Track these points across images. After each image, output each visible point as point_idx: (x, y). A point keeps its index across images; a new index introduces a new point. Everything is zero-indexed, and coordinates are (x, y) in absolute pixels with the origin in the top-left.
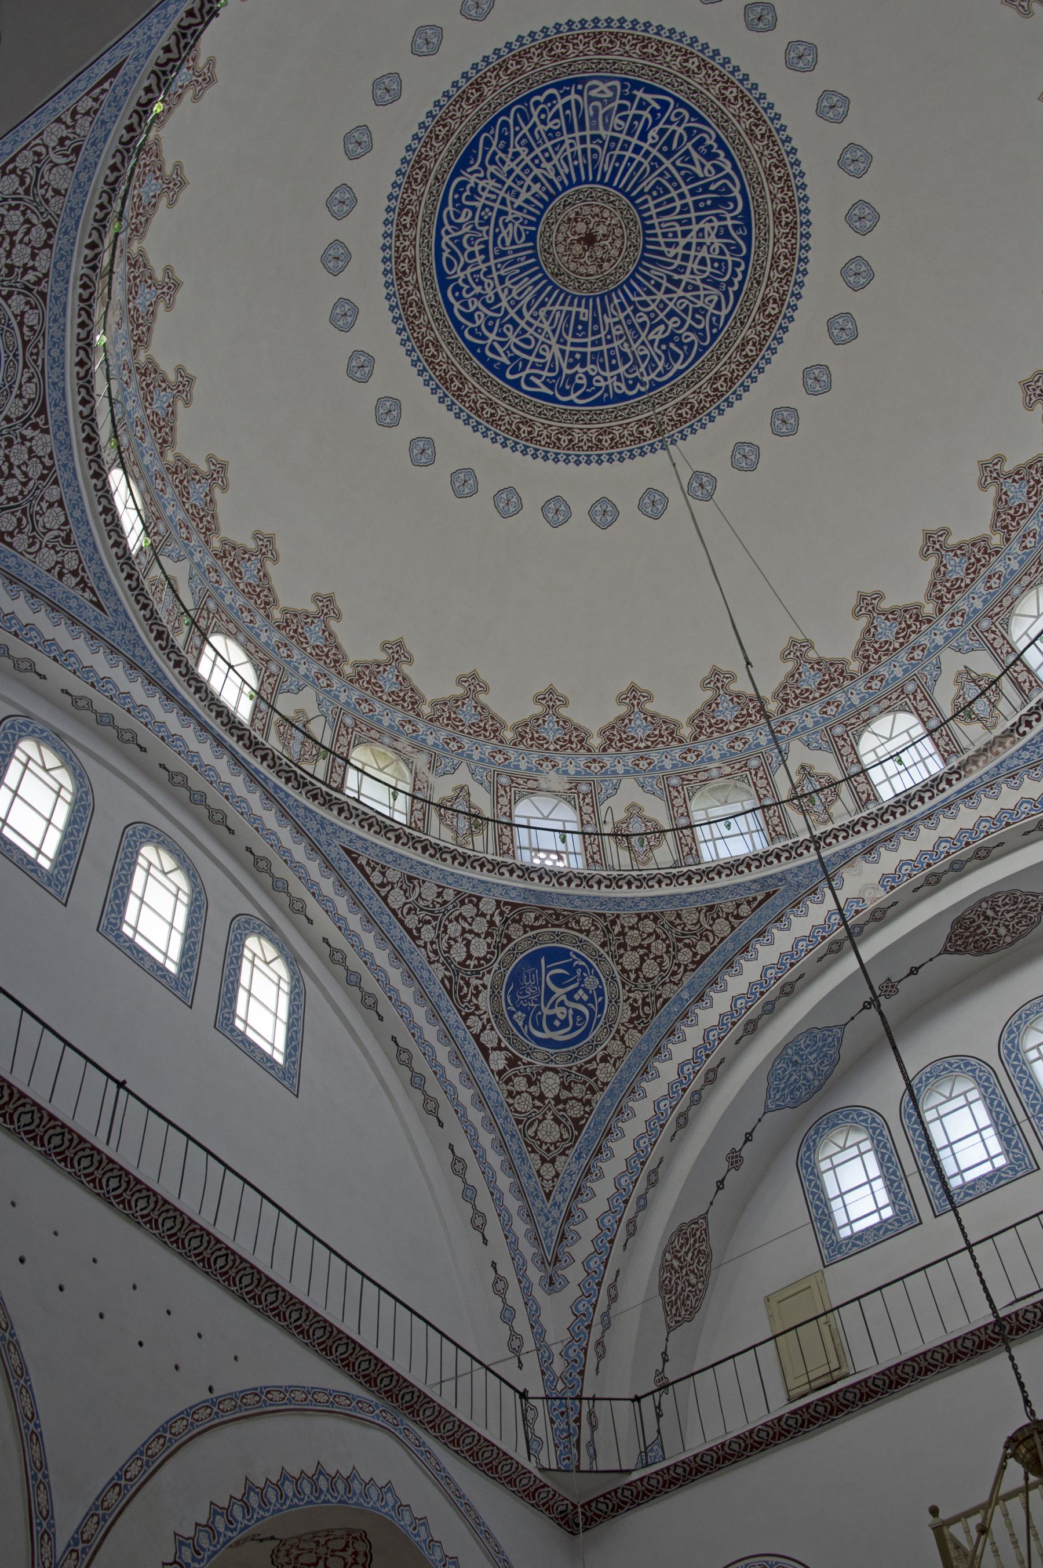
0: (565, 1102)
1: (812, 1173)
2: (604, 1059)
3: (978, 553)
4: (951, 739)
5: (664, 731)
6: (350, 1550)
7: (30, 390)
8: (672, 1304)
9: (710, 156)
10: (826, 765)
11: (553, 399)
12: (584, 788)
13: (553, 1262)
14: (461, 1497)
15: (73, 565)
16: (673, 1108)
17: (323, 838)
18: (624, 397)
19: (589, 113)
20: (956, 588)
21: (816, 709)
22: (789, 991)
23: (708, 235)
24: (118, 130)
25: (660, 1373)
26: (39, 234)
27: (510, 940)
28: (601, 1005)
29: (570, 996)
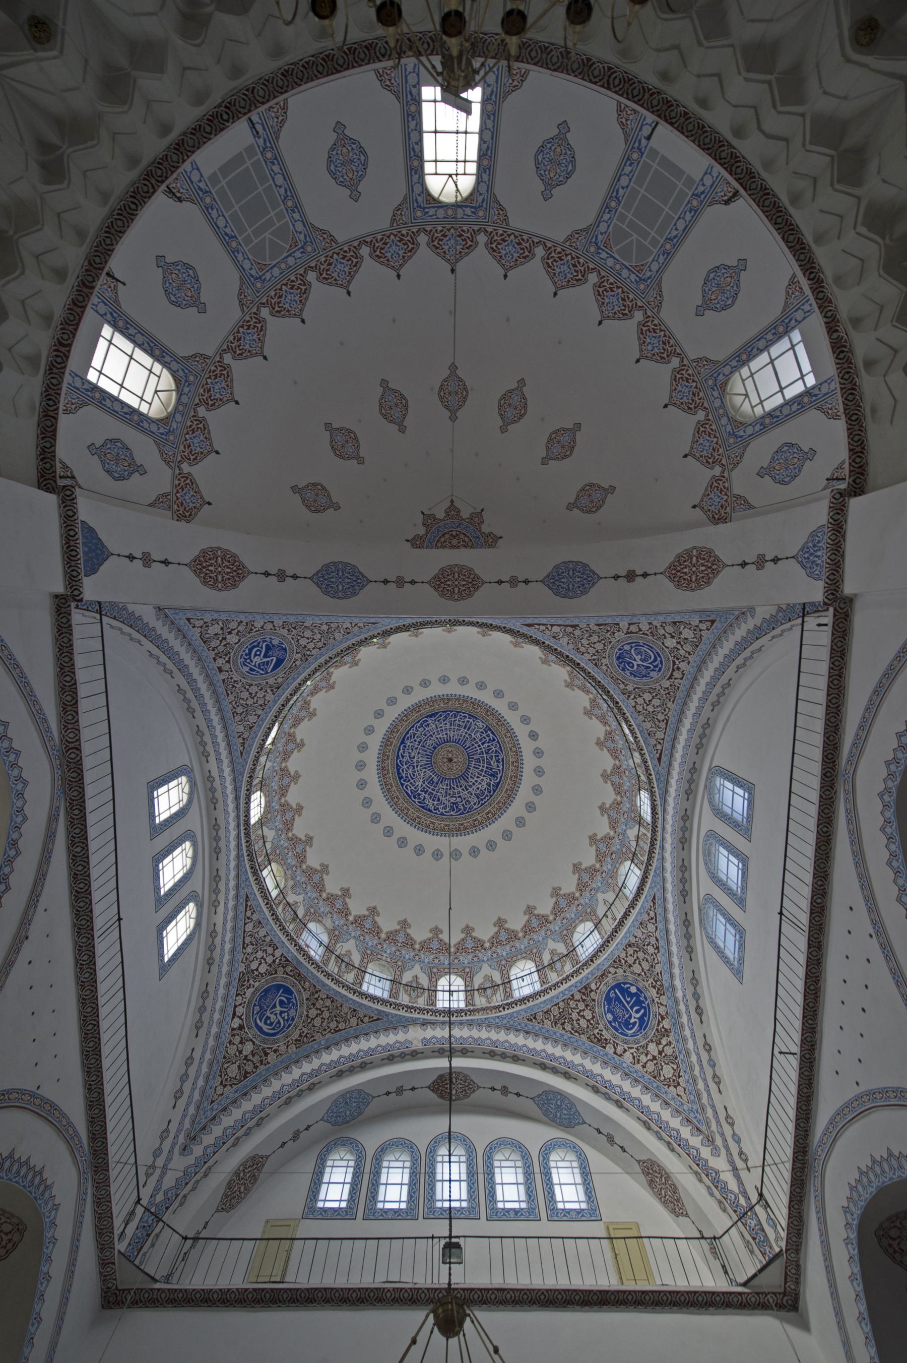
0: (248, 1060)
1: (322, 1164)
2: (275, 1051)
3: (513, 936)
4: (473, 998)
5: (376, 930)
6: (10, 1237)
7: (280, 680)
8: (227, 1196)
9: (498, 761)
10: (424, 981)
11: (410, 797)
12: (337, 933)
13: (193, 1138)
14: (78, 1240)
15: (245, 736)
16: (289, 1092)
17: (243, 885)
18: (430, 811)
19: (473, 727)
20: (500, 943)
21: (431, 957)
22: (363, 1067)
23: (484, 782)
24: (363, 637)
25: (199, 1233)
26: (320, 644)
27: (276, 973)
28: (290, 1025)
29: (281, 1013)
